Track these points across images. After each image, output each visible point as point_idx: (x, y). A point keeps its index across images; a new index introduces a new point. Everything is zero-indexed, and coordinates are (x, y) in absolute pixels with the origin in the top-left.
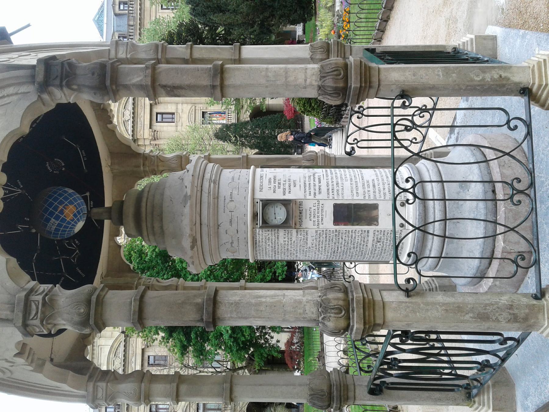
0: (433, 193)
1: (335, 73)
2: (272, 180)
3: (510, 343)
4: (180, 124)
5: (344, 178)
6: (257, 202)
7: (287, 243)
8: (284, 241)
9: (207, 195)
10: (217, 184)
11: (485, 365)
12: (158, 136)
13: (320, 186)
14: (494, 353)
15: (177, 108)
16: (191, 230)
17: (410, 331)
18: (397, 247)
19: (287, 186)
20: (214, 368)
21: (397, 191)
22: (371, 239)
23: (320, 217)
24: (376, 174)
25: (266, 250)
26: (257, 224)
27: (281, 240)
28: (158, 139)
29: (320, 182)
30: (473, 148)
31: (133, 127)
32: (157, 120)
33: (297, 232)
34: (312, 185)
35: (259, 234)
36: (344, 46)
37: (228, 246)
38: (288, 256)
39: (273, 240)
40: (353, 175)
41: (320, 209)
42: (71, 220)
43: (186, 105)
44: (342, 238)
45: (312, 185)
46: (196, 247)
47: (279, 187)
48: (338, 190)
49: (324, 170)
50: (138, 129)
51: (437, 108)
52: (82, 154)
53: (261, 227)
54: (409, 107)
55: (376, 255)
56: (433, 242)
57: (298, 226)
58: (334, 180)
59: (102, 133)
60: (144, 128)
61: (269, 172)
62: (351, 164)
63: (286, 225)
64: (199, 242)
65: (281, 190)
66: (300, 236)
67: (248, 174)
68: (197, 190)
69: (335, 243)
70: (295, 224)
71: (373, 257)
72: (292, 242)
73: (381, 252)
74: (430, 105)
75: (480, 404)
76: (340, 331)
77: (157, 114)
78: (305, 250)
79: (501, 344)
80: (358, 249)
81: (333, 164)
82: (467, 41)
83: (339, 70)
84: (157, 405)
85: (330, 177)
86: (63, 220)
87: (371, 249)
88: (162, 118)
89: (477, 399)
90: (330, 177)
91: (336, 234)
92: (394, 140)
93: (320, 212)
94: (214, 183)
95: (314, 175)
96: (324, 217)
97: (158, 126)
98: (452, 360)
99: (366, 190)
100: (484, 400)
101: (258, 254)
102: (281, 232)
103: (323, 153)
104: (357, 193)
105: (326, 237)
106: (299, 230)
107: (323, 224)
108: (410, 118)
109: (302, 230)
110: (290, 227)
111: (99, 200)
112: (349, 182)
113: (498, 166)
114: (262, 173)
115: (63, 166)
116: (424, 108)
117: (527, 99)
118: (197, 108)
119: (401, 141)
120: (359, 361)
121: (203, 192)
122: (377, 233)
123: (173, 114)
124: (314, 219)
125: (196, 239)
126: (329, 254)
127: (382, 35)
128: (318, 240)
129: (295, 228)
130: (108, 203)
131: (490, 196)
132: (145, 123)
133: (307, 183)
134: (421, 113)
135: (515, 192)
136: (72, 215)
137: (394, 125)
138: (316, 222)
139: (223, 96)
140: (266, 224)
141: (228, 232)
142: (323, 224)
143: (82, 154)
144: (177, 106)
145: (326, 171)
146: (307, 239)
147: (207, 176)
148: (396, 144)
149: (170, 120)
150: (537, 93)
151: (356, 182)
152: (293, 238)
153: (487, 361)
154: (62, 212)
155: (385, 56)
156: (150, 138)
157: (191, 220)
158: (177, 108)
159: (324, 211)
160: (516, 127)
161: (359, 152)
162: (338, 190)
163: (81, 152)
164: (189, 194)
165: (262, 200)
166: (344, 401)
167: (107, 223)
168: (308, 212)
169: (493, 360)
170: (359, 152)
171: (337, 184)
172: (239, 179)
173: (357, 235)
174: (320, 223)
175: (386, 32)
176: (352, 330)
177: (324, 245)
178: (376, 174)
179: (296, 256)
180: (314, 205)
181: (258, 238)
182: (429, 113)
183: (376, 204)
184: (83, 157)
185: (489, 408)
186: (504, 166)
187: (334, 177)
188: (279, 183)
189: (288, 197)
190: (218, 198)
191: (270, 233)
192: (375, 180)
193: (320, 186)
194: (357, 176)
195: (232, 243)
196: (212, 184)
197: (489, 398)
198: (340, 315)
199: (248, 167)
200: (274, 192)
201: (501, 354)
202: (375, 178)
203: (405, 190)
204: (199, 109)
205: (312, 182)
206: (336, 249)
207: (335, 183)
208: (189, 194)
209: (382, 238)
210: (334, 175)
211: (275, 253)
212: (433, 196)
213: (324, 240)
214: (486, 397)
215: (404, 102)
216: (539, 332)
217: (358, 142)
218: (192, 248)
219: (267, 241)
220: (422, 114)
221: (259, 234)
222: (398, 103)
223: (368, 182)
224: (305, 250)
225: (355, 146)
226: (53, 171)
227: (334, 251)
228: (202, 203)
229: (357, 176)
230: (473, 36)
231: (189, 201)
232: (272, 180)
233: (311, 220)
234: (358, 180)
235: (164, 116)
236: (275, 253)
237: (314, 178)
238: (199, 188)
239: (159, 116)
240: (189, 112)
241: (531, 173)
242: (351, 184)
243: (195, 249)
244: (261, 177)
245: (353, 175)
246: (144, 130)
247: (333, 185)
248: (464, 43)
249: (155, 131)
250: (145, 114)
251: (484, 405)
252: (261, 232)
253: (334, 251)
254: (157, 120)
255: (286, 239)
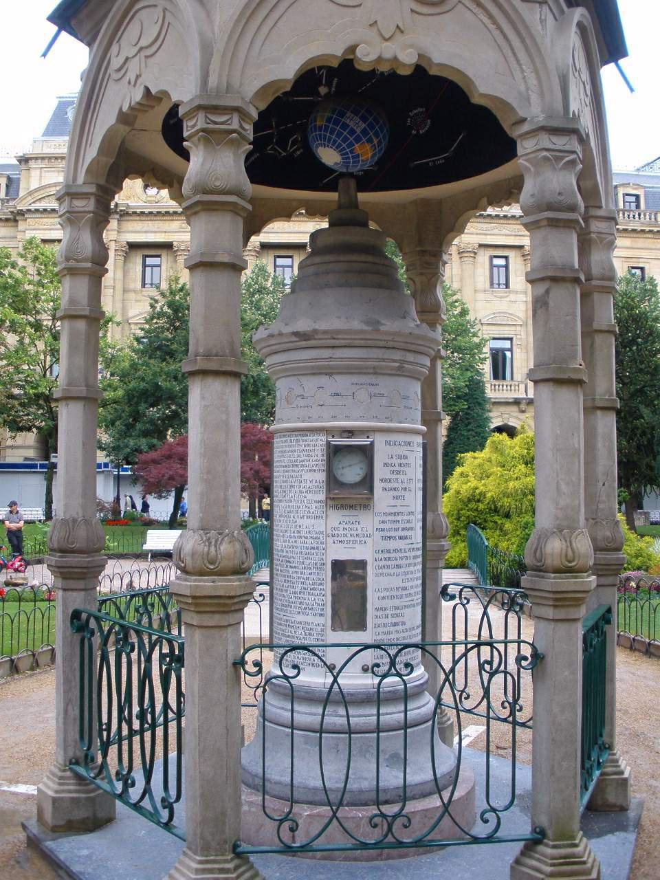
0: (387, 714)
1: (570, 553)
2: (403, 461)
3: (165, 814)
4: (489, 297)
5: (407, 577)
6: (368, 437)
7: (303, 485)
8: (306, 481)
9: (380, 356)
10: (398, 373)
11: (128, 782)
12: (466, 259)
13: (394, 538)
14: (147, 791)
15: (517, 292)
16: (325, 332)
17: (183, 666)
18: (305, 648)
19: (395, 485)
20: (51, 366)
21: (393, 651)
22: (310, 619)
23: (346, 539)
24: (412, 629)
25: (292, 451)
26: (333, 437)
27: (307, 476)
28: (461, 258)
29: (401, 538)
30: (454, 774)
31: (45, 210)
32: (496, 257)
33: (320, 502)
34: (397, 526)
35: (317, 440)
36: (617, 575)
37: (298, 391)
38: (281, 487)
39: (307, 463)
40: (412, 591)
41: (357, 539)
42: (353, 150)
43: (524, 309)
44: (310, 574)
45: (397, 526)
46: (297, 339)
47: (392, 472)
48: (388, 567)
49: (420, 545)
50: (475, 224)
51: (517, 727)
52: (440, 159)
53: (328, 443)
54: (520, 666)
55: (284, 628)
56: (306, 714)
57: (330, 502)
58: (404, 562)
59: (473, 190)
60: (480, 234)
61: (416, 457)
62: (428, 593)
63: (333, 482)
64: (303, 343)
65: (388, 476)
66: (314, 507)
67: (413, 421)
68: (387, 341)
69: (303, 563)
70: (333, 498)
71: (280, 624)
72: (305, 494)
73: (289, 636)
74: (521, 717)
75: (61, 778)
76: (183, 562)
77: (506, 258)
78: (292, 515)
79: (163, 800)
80: (293, 600)
81: (428, 565)
82: (619, 766)
83: (573, 561)
84: (159, 266)
85: (408, 554)
86: (358, 140)
87: (293, 620)
88: (498, 267)
89: (68, 774)
90: (408, 554)
91: (318, 564)
92: (466, 644)
93: (352, 539)
94: (400, 368)
95: (412, 529)
96: (346, 545)
97: (484, 257)
98: (123, 742)
99: (388, 612)
100: (68, 784)
101: (284, 439)
102: (321, 476)
103: (446, 548)
104: (384, 598)
105: (313, 548)
106: (324, 505)
107: (334, 543)
108: (502, 668)
109: (324, 509)
110: (329, 490)
111: (367, 182)
112: (402, 585)
113: (425, 808)
114: (415, 444)
115: (418, 132)
116: (518, 707)
117: (529, 837)
118: (519, 328)
119: (464, 659)
120: (114, 600)
121: (383, 350)
122: (319, 628)
123: (507, 285)
124: (341, 529)
125: (309, 340)
126: (284, 554)
127: (639, 651)
128: (308, 535)
129: (326, 498)
130: (363, 197)
131: (382, 797)
132: (488, 237)
133: (399, 518)
134: (510, 703)
135: (389, 819)
136: (360, 152)
137: (490, 644)
138: (337, 532)
139: (536, 382)
140: (334, 452)
141: (321, 390)
142: (334, 543)
143: (440, 159)
144: (521, 292)
145: (418, 549)
146: (309, 517)
147: (410, 357)
148: (460, 649)
149: (496, 281)
150: (536, 853)
151: (402, 596)
152: (310, 495)
153: (133, 785)
154: (370, 141)
155: (598, 636)
156: (462, 245)
157: (338, 332)
158: (517, 292)
159: (355, 546)
160: (486, 821)
161: (447, 605)
162: (388, 567)
163: (443, 158)
164: (382, 328)
165: (372, 444)
166: (61, 573)
167: (334, 196)
168: (352, 519)
169: (135, 793)
170: (447, 605)
171: (399, 566)
172: (405, 407)
173: (316, 598)
174: (336, 538)
175: (645, 658)
176: (186, 580)
177: (299, 545)
178: (412, 629)
179: (281, 501)
180: (364, 529)
181: (311, 438)
182: (509, 717)
183: (366, 627)
184: (433, 161)
185: (57, 792)
186: (426, 816)
187: (409, 562)
188: (399, 473)
189: (378, 485)
190: (375, 373)
191: (320, 458)
192: (404, 627)
193: (394, 538)
194: (411, 598)
195: (303, 397)
196: (397, 364)
197: (70, 791)
198: (206, 562)
199: (424, 423)
200: (385, 464)
201: (146, 803)
202: (408, 626)
203: (393, 663)
204: (518, 333)
205: (402, 526)
206: (294, 565)
207: (399, 562)
208: (382, 328)
209: (312, 638)
210: (412, 561)
211: (286, 466)
212: (384, 714)
213: (307, 545)
214: (72, 787)
215: (525, 658)
216: (185, 849)
217: (464, 605)
218: (296, 334)
219: (306, 453)
220: (508, 708)
221: (317, 440)
222: (527, 651)
223: (402, 615)
224: (292, 515)
225: (457, 600)
226: (411, 117)
227: (289, 562)
228: (369, 349)
229: (411, 598)
230: (626, 775)
231: (370, 328)
232: (403, 461)
233: (340, 523)
234: (404, 599)
235: (503, 270)
236: (286, 466)
237: (408, 529)
238: (391, 344)
239: (502, 262)
240: (511, 314)
241: (421, 845)
242: (398, 589)
243: (294, 339)
244: (409, 443)
245: (412, 591)
246: (477, 234)
247: (396, 559)
248: (617, 761)
249: (475, 253)
250: (504, 237)
251: (60, 784)
252: (322, 443)
253: (289, 562)
254: (496, 257)
255: (309, 484)
